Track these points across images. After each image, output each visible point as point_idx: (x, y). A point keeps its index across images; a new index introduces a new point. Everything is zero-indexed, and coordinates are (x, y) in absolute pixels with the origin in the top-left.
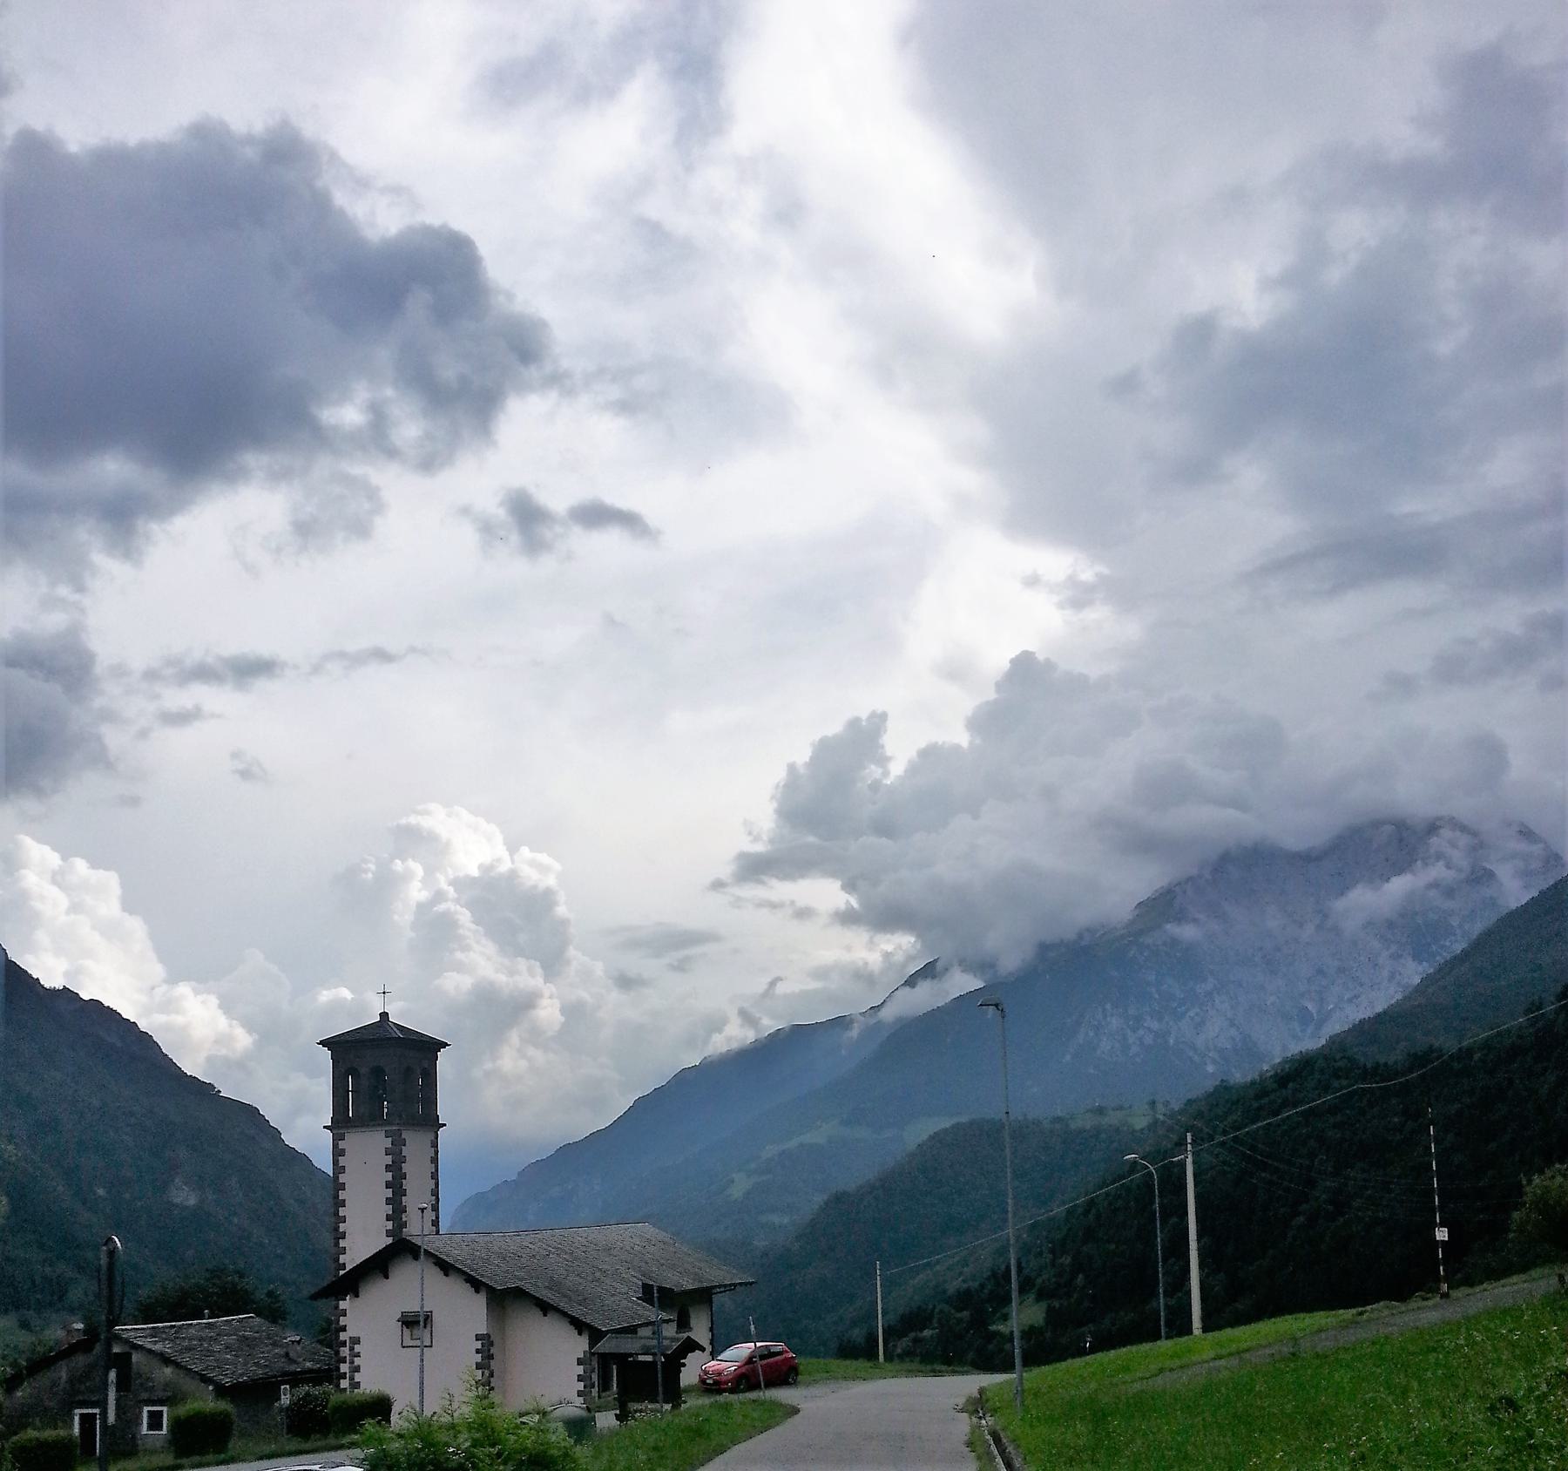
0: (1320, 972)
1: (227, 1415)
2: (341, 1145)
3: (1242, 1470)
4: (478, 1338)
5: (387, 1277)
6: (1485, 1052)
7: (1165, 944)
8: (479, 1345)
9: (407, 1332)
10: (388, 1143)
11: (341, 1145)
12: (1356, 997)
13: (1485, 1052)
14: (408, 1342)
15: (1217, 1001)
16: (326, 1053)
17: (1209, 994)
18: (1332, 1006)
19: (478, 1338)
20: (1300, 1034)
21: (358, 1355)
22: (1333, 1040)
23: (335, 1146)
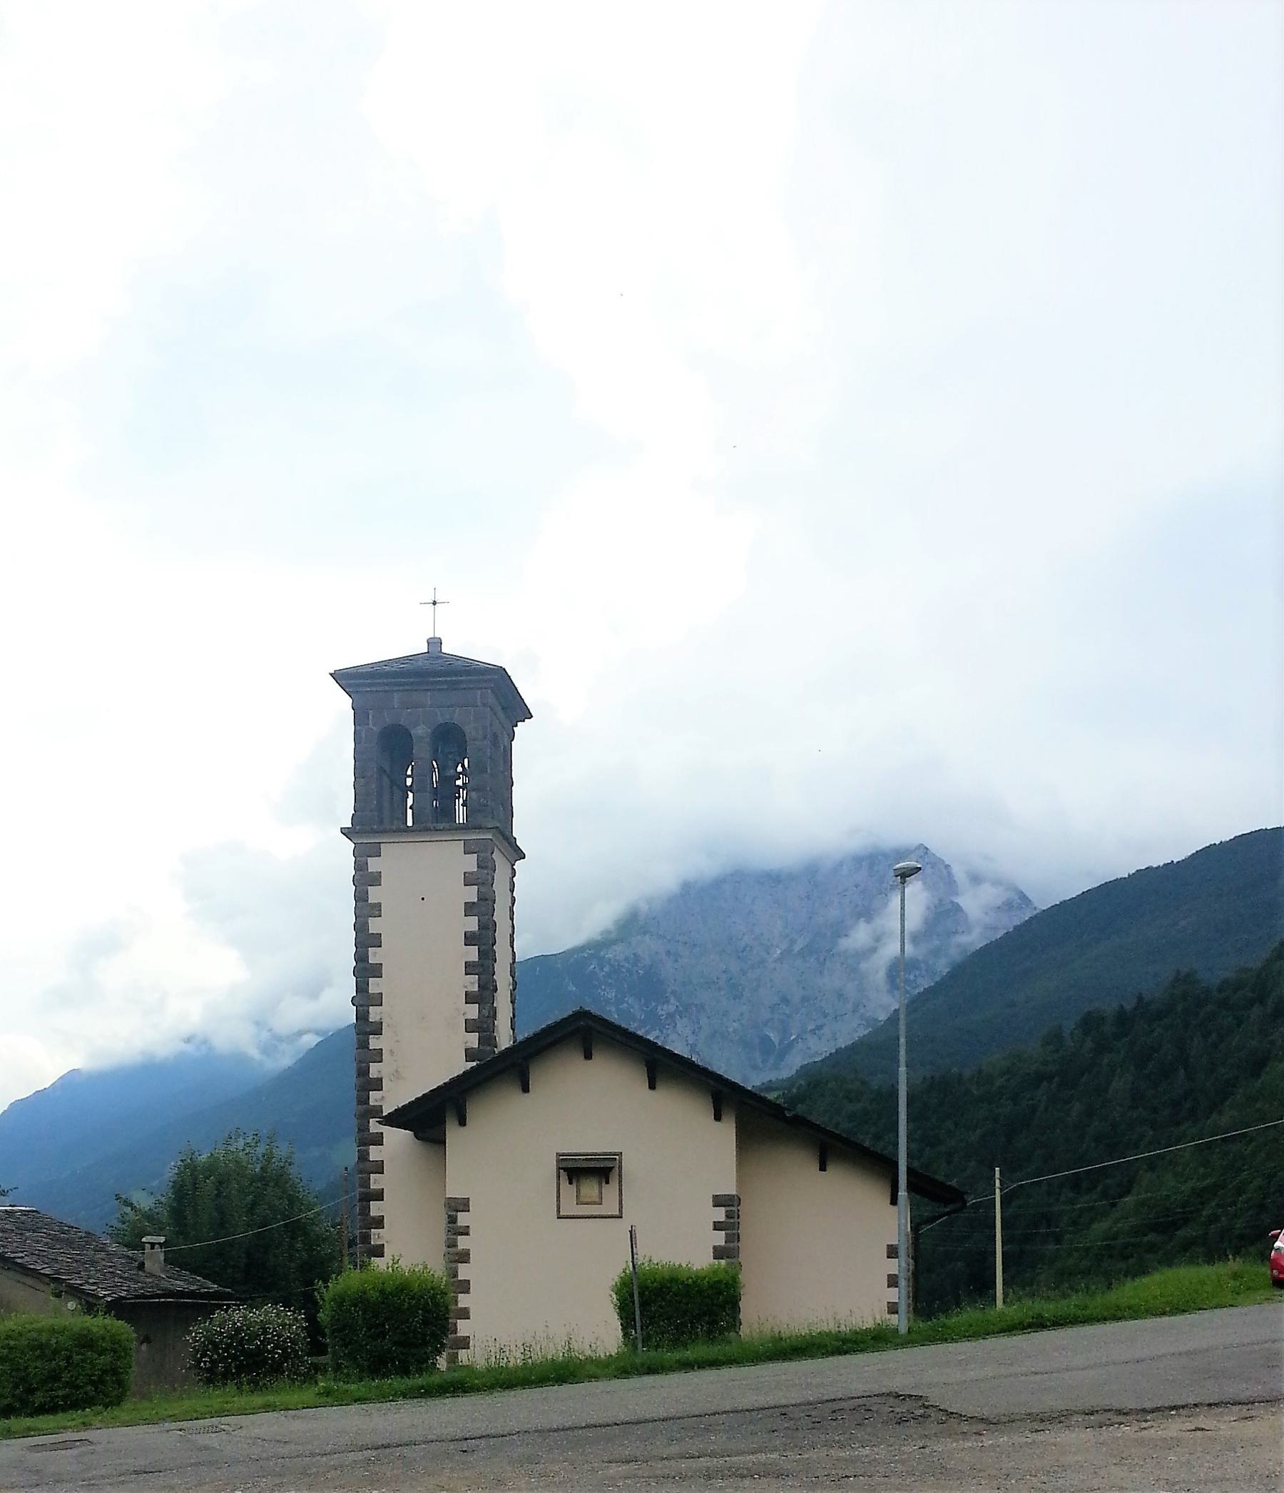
0: (785, 1000)
1: (117, 1348)
2: (373, 865)
3: (972, 1492)
4: (718, 1201)
5: (526, 1089)
6: (1006, 1077)
7: (626, 959)
8: (720, 1214)
9: (569, 1190)
10: (470, 864)
11: (373, 865)
12: (820, 1027)
13: (1006, 1077)
14: (569, 1207)
15: (679, 1025)
16: (342, 703)
17: (670, 1016)
18: (794, 1037)
19: (718, 1201)
20: (761, 1066)
21: (465, 1232)
22: (804, 1071)
23: (360, 867)
